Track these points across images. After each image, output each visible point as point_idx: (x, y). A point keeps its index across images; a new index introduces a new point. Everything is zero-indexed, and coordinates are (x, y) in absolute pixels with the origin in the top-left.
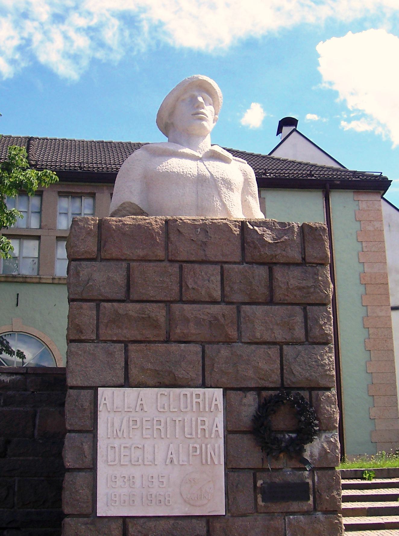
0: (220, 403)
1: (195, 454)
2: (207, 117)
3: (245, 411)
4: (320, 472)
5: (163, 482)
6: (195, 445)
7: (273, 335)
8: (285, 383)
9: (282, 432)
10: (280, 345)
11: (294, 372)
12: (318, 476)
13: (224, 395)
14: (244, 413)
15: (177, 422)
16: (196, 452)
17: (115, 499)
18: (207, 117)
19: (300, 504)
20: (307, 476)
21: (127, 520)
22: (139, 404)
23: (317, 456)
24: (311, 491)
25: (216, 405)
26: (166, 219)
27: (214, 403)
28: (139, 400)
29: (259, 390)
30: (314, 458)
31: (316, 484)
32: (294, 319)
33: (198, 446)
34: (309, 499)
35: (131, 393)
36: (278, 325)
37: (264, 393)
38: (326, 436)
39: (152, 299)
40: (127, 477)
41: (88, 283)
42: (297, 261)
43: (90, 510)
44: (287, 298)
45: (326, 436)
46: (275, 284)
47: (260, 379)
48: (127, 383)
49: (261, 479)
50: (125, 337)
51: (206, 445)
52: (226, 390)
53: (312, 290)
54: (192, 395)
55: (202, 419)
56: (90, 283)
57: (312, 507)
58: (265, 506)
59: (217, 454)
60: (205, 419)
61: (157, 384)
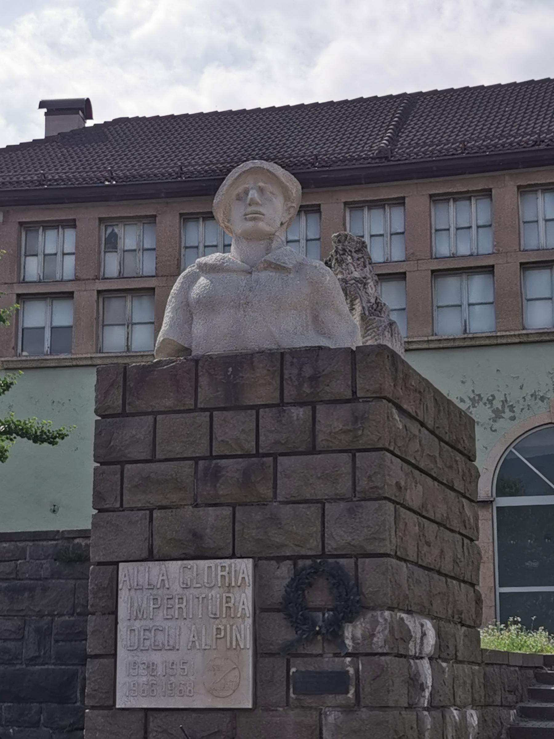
0: (248, 576)
1: (219, 636)
2: (263, 215)
3: (277, 585)
4: (364, 658)
5: (184, 669)
6: (220, 626)
7: (313, 491)
8: (326, 550)
9: (318, 609)
10: (321, 503)
11: (334, 536)
12: (363, 664)
13: (255, 566)
14: (276, 587)
15: (201, 599)
16: (220, 634)
17: (134, 689)
18: (263, 215)
19: (337, 697)
20: (348, 663)
21: (149, 713)
22: (160, 580)
23: (361, 639)
24: (353, 682)
25: (243, 578)
26: (455, 252)
27: (241, 576)
28: (161, 575)
29: (294, 559)
30: (356, 641)
31: (360, 674)
32: (337, 471)
33: (222, 628)
34: (347, 693)
35: (155, 567)
36: (319, 478)
37: (301, 563)
38: (372, 615)
39: (179, 456)
40: (146, 664)
41: (110, 443)
42: (344, 397)
43: (111, 703)
44: (331, 444)
45: (372, 615)
46: (318, 427)
47: (296, 545)
48: (151, 557)
49: (293, 667)
50: (149, 503)
51: (231, 626)
52: (257, 560)
53: (360, 432)
54: (216, 567)
55: (228, 595)
56: (112, 444)
57: (353, 701)
58: (296, 699)
59: (243, 636)
60: (230, 595)
61: (183, 556)
